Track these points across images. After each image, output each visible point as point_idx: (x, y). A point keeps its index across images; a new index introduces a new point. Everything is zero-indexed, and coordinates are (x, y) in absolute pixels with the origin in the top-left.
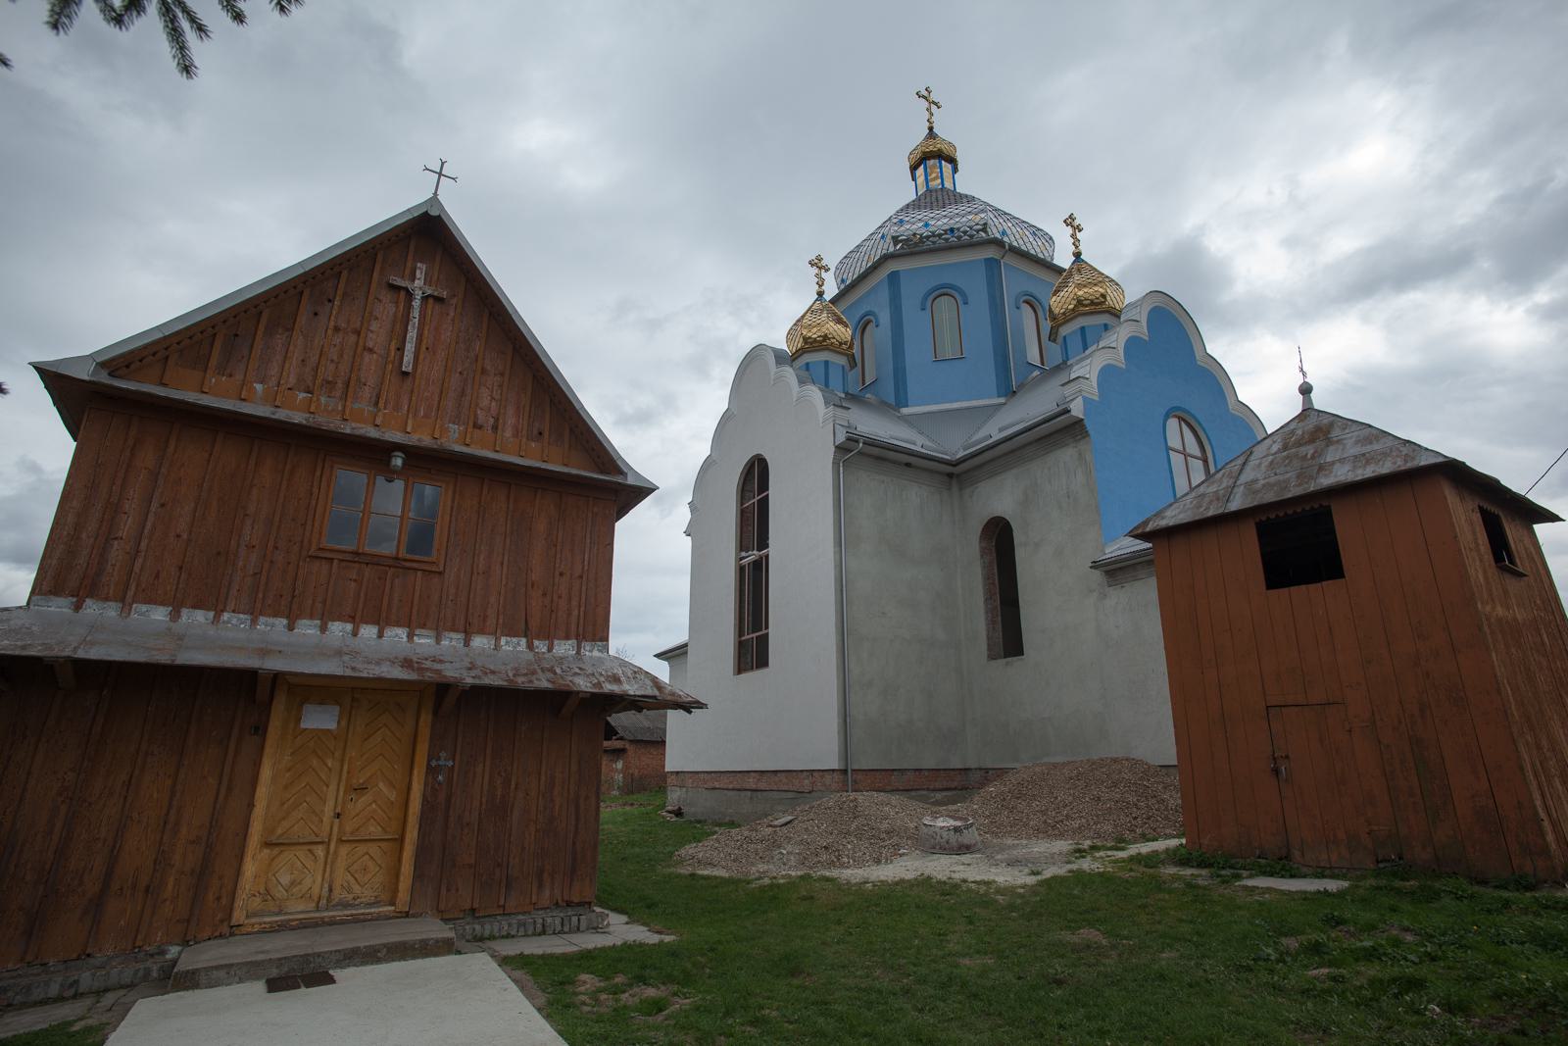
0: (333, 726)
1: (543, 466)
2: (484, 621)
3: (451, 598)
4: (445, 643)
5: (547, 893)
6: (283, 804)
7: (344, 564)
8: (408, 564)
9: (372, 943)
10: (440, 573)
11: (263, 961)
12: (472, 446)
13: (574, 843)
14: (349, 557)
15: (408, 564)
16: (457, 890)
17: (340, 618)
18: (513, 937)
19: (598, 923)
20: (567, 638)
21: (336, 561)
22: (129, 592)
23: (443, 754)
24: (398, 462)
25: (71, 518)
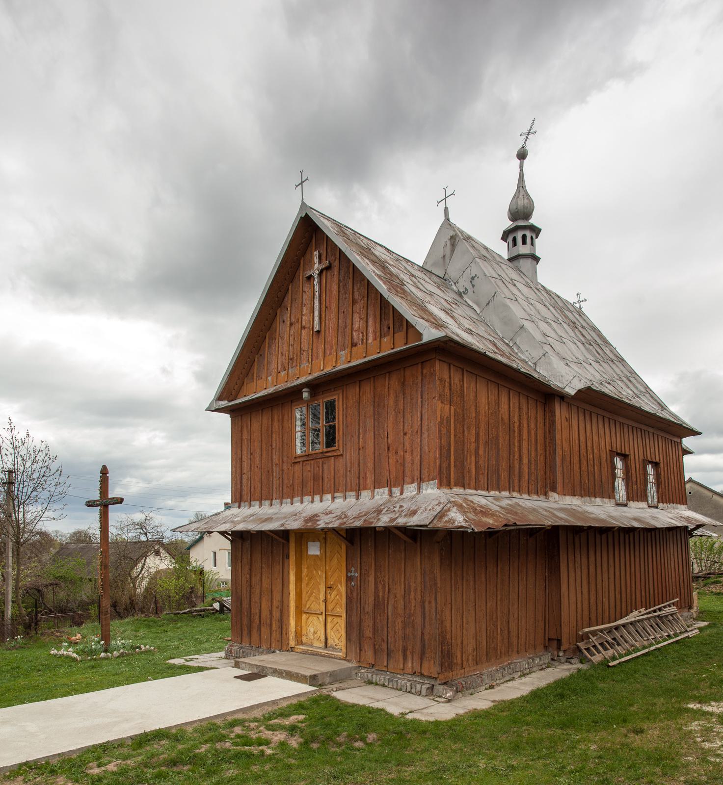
0: (318, 553)
1: (366, 359)
2: (366, 480)
3: (349, 469)
4: (377, 497)
5: (410, 665)
6: (307, 593)
7: (305, 463)
8: (327, 455)
9: (289, 669)
10: (342, 455)
11: (630, 659)
12: (352, 361)
13: (423, 634)
14: (305, 458)
15: (327, 455)
16: (365, 651)
17: (307, 495)
18: (386, 686)
19: (443, 694)
20: (412, 482)
21: (301, 462)
22: (643, 425)
23: (353, 569)
24: (305, 395)
25: (234, 469)
